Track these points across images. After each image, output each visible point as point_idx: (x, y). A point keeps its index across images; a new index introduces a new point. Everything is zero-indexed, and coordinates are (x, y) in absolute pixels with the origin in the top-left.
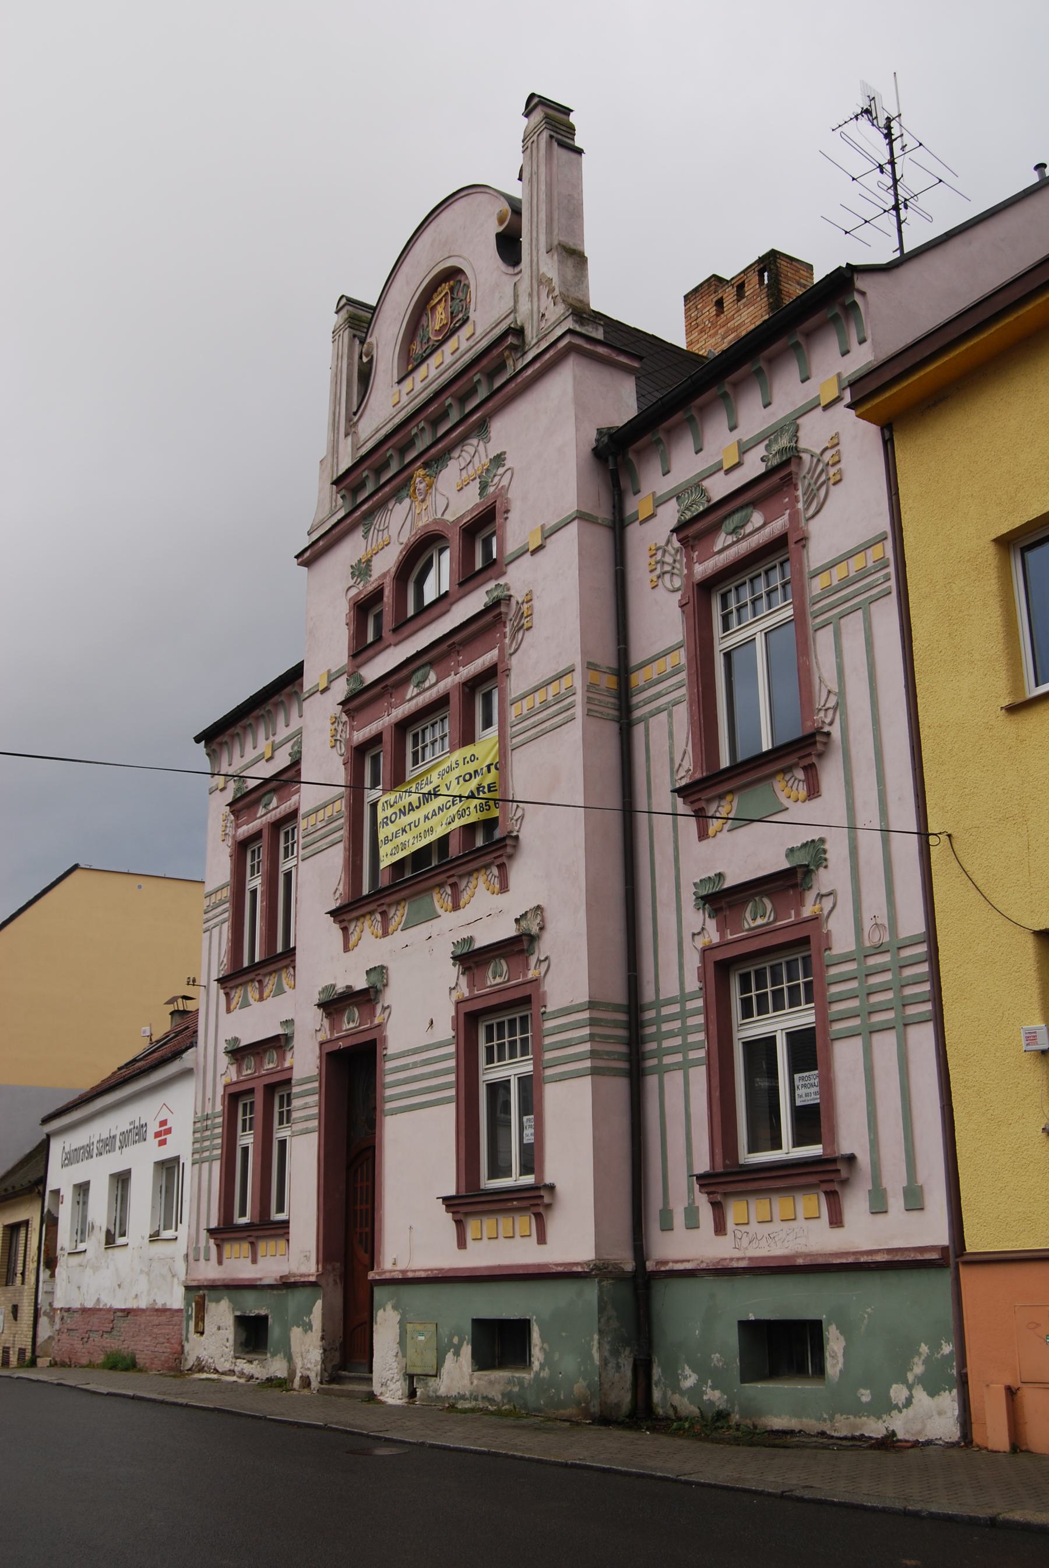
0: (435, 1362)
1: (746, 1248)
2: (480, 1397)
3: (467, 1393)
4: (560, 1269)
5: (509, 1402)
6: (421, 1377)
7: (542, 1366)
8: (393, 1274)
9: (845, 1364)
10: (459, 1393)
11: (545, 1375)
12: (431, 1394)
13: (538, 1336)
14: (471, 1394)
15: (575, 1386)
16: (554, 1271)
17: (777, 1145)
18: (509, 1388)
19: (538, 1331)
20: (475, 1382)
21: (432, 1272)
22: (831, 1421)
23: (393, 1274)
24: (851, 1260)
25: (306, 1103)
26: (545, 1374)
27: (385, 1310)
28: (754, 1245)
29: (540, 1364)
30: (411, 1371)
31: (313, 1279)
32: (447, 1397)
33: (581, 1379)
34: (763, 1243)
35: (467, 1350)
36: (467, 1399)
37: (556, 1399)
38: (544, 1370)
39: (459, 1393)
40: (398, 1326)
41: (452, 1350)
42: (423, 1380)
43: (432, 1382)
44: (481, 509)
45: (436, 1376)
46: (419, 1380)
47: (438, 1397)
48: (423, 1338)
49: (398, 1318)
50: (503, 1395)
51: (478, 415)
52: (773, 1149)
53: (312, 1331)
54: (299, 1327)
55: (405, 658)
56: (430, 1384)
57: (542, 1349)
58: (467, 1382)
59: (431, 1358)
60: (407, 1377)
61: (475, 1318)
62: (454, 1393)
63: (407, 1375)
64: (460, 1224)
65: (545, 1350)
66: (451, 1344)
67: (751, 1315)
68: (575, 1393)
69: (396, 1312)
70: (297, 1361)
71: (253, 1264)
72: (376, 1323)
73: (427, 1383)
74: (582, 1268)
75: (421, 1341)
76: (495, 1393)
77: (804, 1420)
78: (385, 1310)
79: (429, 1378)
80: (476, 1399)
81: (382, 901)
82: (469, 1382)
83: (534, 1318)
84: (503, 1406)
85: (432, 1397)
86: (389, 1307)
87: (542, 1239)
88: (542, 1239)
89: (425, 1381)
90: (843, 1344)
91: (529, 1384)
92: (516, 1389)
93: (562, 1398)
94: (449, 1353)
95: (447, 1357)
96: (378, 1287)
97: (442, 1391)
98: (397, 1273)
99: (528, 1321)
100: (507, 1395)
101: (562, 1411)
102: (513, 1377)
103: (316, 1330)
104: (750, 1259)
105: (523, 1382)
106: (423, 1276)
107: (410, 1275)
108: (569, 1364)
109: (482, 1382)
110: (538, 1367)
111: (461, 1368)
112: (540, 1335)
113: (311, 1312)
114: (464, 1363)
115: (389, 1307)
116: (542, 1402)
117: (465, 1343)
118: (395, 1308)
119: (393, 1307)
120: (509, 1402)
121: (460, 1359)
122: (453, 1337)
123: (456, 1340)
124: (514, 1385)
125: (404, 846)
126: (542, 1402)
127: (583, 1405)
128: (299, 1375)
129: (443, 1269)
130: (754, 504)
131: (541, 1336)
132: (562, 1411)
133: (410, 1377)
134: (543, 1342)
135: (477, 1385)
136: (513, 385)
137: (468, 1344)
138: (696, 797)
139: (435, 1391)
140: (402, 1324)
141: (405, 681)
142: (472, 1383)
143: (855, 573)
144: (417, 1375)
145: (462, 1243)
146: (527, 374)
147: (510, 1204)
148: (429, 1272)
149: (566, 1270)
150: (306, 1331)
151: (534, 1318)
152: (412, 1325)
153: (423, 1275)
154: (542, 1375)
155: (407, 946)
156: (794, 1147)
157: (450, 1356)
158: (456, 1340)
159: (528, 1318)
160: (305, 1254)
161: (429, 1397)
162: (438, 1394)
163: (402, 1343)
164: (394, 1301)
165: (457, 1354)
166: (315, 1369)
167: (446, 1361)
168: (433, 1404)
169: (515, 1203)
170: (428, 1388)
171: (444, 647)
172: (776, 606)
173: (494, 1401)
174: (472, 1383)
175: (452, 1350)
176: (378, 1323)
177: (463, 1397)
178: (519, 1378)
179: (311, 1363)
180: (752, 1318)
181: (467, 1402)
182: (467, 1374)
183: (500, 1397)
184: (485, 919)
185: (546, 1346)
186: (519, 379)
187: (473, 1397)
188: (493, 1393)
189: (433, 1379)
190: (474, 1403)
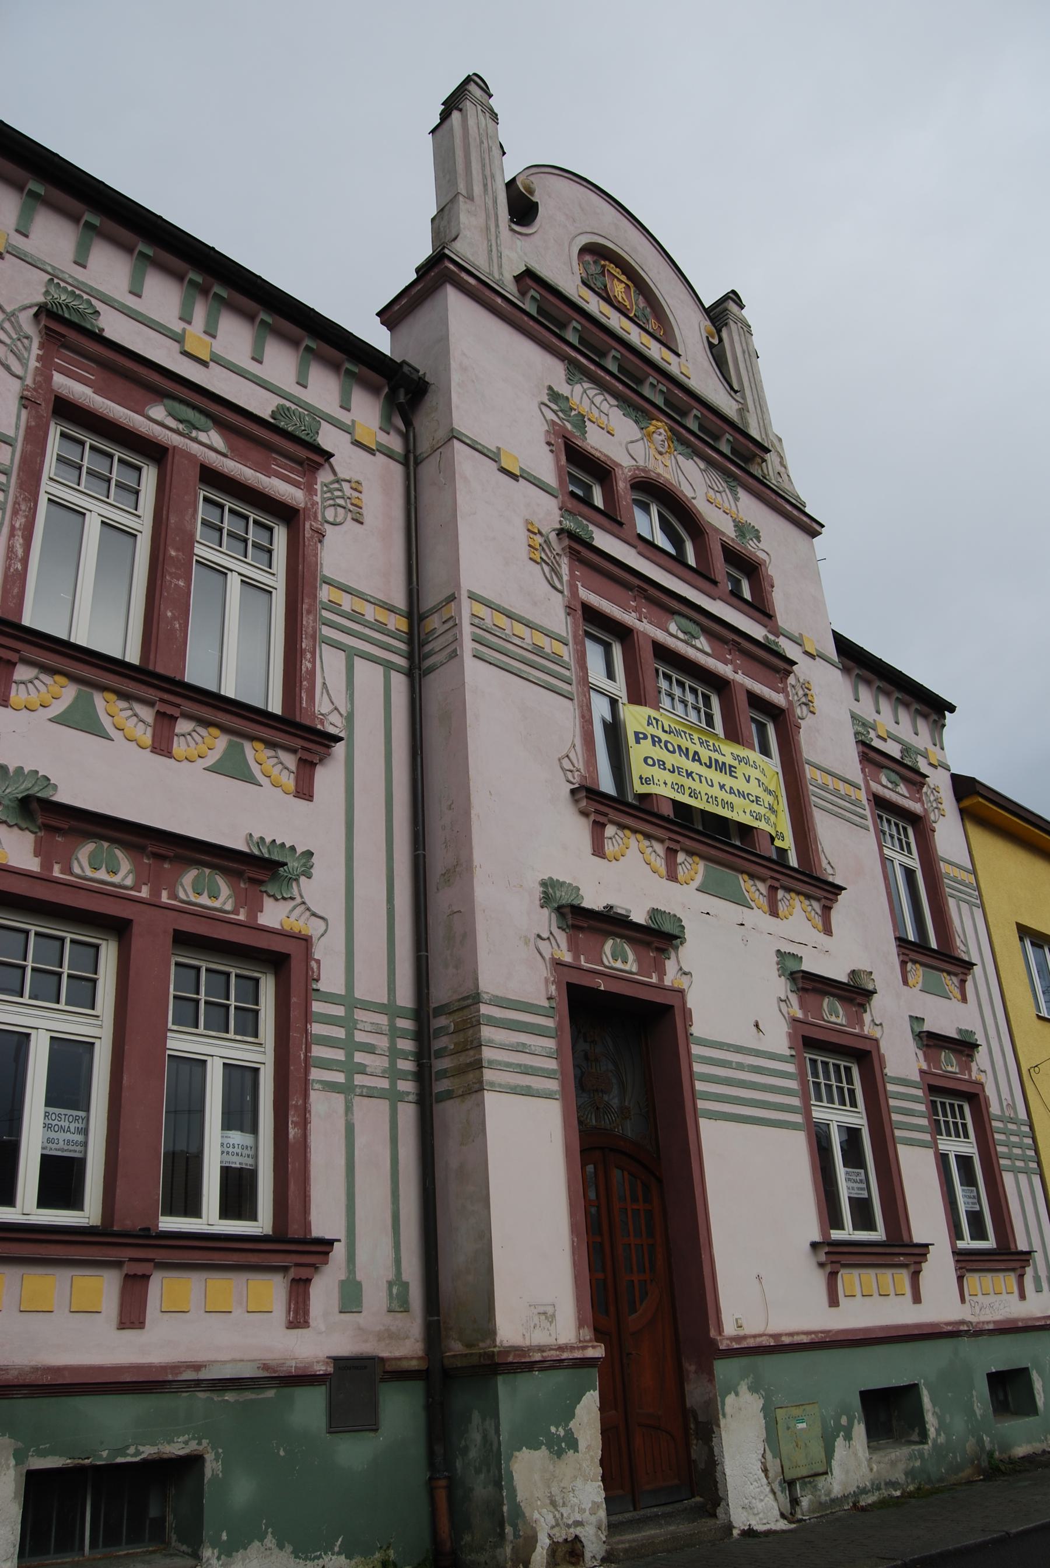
0: (823, 1454)
1: (979, 1315)
2: (883, 1484)
3: (868, 1484)
4: (950, 1328)
5: (913, 1479)
6: (807, 1480)
7: (938, 1432)
8: (758, 1340)
9: (1045, 1397)
10: (858, 1487)
11: (943, 1441)
12: (823, 1498)
13: (929, 1400)
14: (873, 1484)
15: (967, 1445)
16: (945, 1330)
17: (193, 1209)
18: (912, 1465)
19: (928, 1395)
20: (875, 1468)
21: (817, 1336)
22: (1047, 1441)
23: (758, 1340)
24: (1043, 1323)
25: (524, 1045)
26: (941, 1439)
27: (737, 1394)
28: (983, 1312)
29: (936, 1429)
30: (790, 1475)
31: (414, 1364)
32: (845, 1497)
33: (970, 1437)
34: (988, 1311)
35: (859, 1430)
36: (869, 1491)
37: (954, 1463)
38: (940, 1435)
39: (858, 1487)
40: (762, 1415)
41: (842, 1433)
42: (810, 1482)
43: (821, 1482)
44: (743, 552)
45: (826, 1473)
46: (804, 1485)
47: (833, 1501)
48: (804, 1425)
49: (761, 1402)
50: (906, 1474)
51: (737, 471)
52: (186, 1214)
53: (576, 1450)
54: (537, 1448)
55: (699, 604)
56: (820, 1485)
57: (934, 1413)
58: (864, 1469)
59: (817, 1450)
60: (786, 1485)
61: (862, 1389)
62: (852, 1489)
63: (785, 1481)
64: (832, 1279)
65: (937, 1414)
66: (839, 1427)
67: (992, 1368)
68: (968, 1452)
69: (755, 1395)
70: (536, 1515)
71: (830, 1306)
72: (724, 1415)
73: (815, 1487)
74: (968, 1326)
75: (802, 1429)
76: (899, 1476)
77: (1034, 1444)
78: (737, 1394)
79: (817, 1478)
80: (879, 1489)
81: (679, 838)
82: (868, 1470)
83: (922, 1381)
84: (907, 1487)
85: (826, 1502)
86: (743, 1388)
87: (917, 1299)
88: (917, 1299)
89: (813, 1484)
90: (1041, 1383)
91: (929, 1454)
92: (918, 1464)
93: (959, 1460)
94: (838, 1440)
95: (836, 1443)
96: (719, 1361)
97: (837, 1490)
98: (764, 1338)
99: (912, 1389)
100: (910, 1473)
101: (961, 1475)
102: (913, 1450)
103: (589, 1447)
104: (994, 1322)
105: (924, 1453)
106: (805, 1341)
107: (787, 1340)
108: (959, 1424)
109: (882, 1465)
110: (935, 1434)
111: (856, 1455)
112: (930, 1399)
113: (569, 1414)
114: (858, 1447)
115: (743, 1388)
116: (943, 1471)
117: (856, 1421)
118: (753, 1389)
119: (749, 1388)
120: (913, 1482)
121: (853, 1442)
122: (841, 1418)
123: (844, 1421)
124: (916, 1459)
125: (693, 794)
126: (943, 1471)
127: (976, 1462)
128: (543, 1542)
129: (830, 1331)
130: (221, 425)
131: (931, 1400)
132: (961, 1475)
133: (790, 1484)
134: (934, 1406)
135: (877, 1471)
136: (774, 496)
137: (859, 1424)
138: (907, 952)
139: (829, 1493)
140: (768, 1411)
141: (161, 395)
142: (871, 1470)
143: (394, 630)
144: (798, 1479)
145: (834, 1301)
146: (706, 449)
147: (897, 1259)
148: (813, 1336)
149: (955, 1329)
150: (560, 1454)
151: (922, 1381)
152: (784, 1410)
153: (805, 1339)
154: (939, 1441)
155: (708, 913)
156: (200, 1217)
157: (840, 1442)
158: (844, 1421)
159: (916, 1382)
160: (541, 1309)
161: (820, 1503)
162: (833, 1496)
163: (772, 1439)
164: (750, 1379)
165: (848, 1437)
166: (593, 1519)
167: (836, 1449)
168: (828, 1512)
169: (902, 1258)
170: (818, 1493)
171: (731, 636)
172: (86, 478)
173: (899, 1484)
174: (871, 1470)
175: (842, 1433)
176: (728, 1416)
177: (863, 1491)
178: (919, 1451)
179: (582, 1511)
180: (994, 1370)
181: (869, 1494)
182: (864, 1459)
183: (903, 1477)
184: (810, 947)
185: (937, 1410)
186: (779, 500)
187: (874, 1487)
188: (897, 1475)
189: (823, 1478)
190: (877, 1494)
